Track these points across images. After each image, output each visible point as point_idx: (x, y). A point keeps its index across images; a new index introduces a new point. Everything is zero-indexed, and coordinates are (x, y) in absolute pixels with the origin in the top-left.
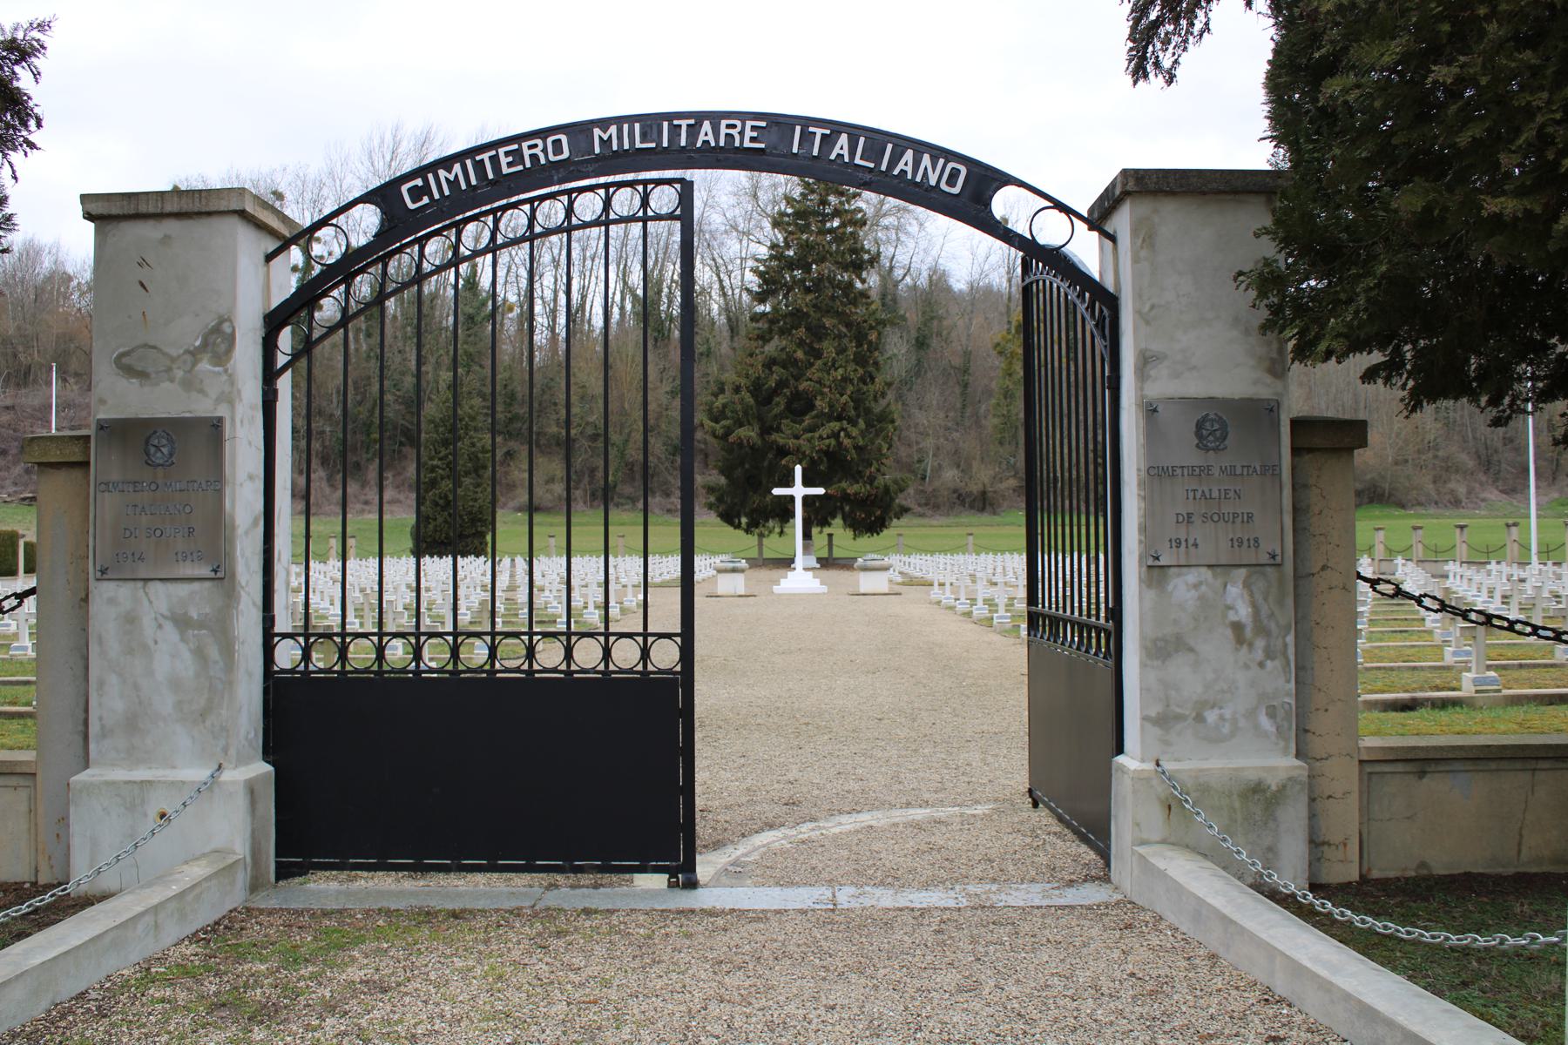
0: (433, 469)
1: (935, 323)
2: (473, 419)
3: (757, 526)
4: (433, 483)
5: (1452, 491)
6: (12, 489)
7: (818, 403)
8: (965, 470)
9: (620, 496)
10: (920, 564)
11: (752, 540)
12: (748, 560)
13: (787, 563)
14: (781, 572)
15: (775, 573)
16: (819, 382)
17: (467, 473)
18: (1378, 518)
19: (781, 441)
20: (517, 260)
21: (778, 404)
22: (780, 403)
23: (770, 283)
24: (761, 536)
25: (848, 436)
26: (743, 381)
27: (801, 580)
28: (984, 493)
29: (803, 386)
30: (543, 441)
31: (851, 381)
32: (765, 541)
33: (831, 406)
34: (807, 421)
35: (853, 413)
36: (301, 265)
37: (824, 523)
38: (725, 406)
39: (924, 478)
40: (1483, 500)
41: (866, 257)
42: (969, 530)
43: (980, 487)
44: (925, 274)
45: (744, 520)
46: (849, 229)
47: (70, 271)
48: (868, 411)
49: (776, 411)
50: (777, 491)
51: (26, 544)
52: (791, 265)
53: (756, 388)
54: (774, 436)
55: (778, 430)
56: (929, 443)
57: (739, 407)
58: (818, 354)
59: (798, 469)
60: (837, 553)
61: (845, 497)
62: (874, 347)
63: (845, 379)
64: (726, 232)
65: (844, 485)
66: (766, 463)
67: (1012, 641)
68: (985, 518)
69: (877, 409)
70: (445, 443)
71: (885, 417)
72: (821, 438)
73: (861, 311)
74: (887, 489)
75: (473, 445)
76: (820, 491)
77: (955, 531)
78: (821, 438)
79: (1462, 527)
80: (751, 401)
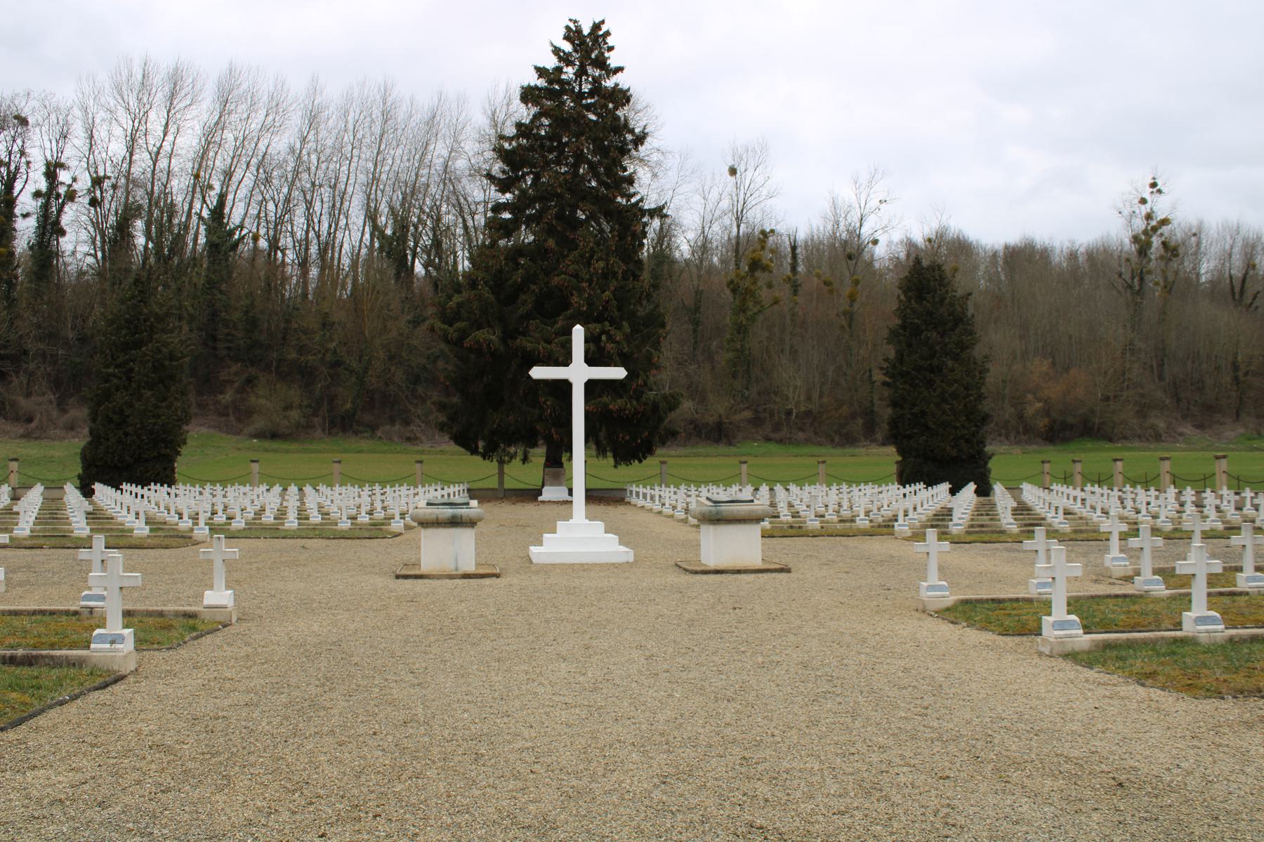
5: (1153, 427)
7: (575, 299)
11: (491, 467)
16: (576, 276)
19: (529, 346)
20: (267, 197)
21: (525, 302)
22: (527, 302)
25: (610, 338)
26: (480, 275)
31: (615, 274)
32: (506, 468)
33: (590, 304)
38: (459, 305)
40: (1181, 434)
41: (629, 137)
45: (481, 444)
49: (522, 310)
53: (498, 282)
54: (521, 342)
55: (524, 334)
68: (722, 449)
74: (655, 407)
75: (159, 351)
80: (492, 297)
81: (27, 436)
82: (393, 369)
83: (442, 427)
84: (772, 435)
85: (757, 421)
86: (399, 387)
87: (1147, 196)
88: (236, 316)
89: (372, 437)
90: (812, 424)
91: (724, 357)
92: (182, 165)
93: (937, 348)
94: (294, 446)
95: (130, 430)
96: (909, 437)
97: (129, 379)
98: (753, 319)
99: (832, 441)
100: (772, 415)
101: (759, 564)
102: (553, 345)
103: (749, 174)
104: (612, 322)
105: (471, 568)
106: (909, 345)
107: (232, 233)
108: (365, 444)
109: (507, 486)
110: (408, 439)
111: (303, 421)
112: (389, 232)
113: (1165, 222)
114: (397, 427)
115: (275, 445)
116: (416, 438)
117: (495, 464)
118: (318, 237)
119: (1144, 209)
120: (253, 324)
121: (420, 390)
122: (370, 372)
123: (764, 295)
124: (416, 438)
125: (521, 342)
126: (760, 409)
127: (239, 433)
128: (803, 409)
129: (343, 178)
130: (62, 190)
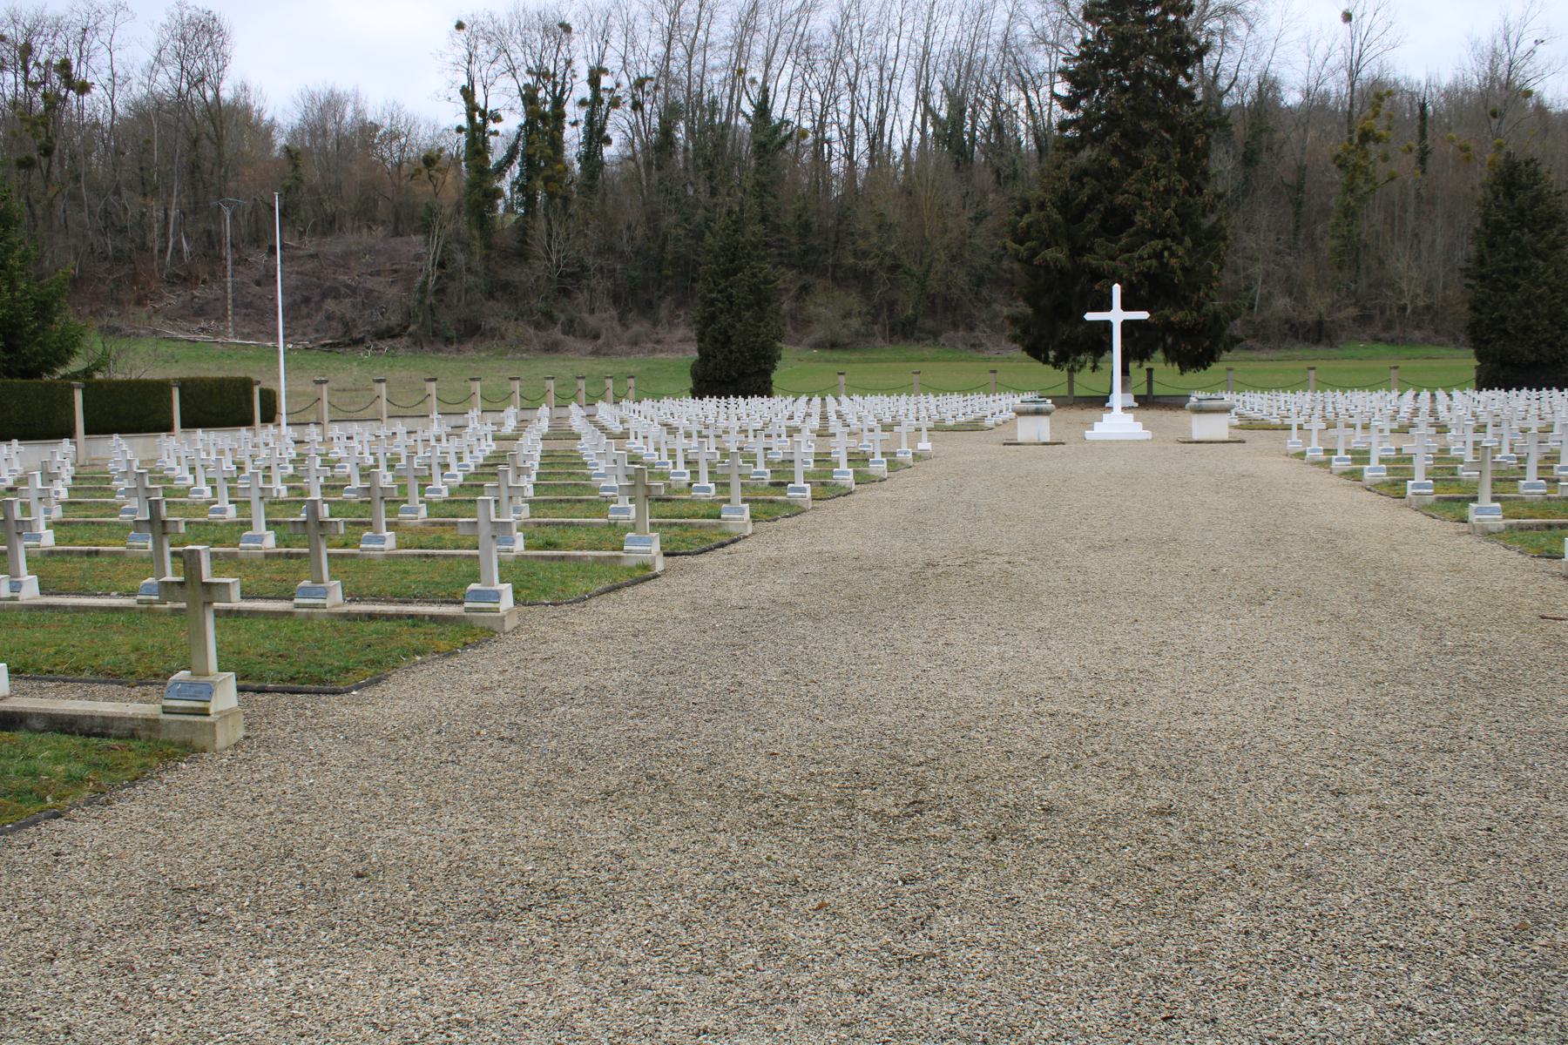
0: (712, 302)
1: (1265, 136)
2: (755, 247)
3: (1066, 361)
4: (712, 318)
6: (312, 336)
7: (1138, 218)
9: (921, 330)
10: (1257, 403)
11: (1062, 375)
12: (1054, 399)
13: (1100, 402)
14: (1095, 412)
16: (1139, 195)
17: (748, 307)
20: (811, 84)
22: (1093, 220)
23: (1082, 78)
24: (1072, 371)
25: (1172, 254)
26: (1048, 197)
27: (1119, 423)
28: (1319, 324)
29: (1120, 199)
30: (840, 274)
32: (1076, 376)
35: (1178, 229)
36: (589, 98)
37: (1143, 356)
38: (1029, 225)
39: (1251, 307)
43: (1315, 317)
44: (1254, 84)
45: (1052, 354)
46: (1172, 17)
47: (370, 118)
48: (1196, 227)
49: (1089, 228)
50: (1090, 316)
51: (262, 392)
52: (1105, 62)
53: (1064, 203)
54: (1088, 259)
55: (1091, 250)
56: (1258, 269)
57: (1044, 226)
58: (1137, 164)
59: (1117, 289)
60: (1158, 390)
61: (1168, 327)
62: (1204, 153)
63: (1169, 191)
64: (1033, 44)
65: (1167, 312)
66: (1078, 289)
67: (1451, 527)
68: (1321, 351)
69: (1207, 222)
70: (727, 274)
71: (1216, 234)
72: (1141, 258)
74: (1216, 318)
75: (754, 275)
76: (1143, 315)
81: (596, 353)
83: (1014, 339)
84: (1382, 335)
85: (1364, 319)
88: (789, 219)
89: (936, 344)
90: (1432, 320)
91: (1329, 245)
92: (718, 59)
94: (856, 356)
95: (734, 347)
96: (1487, 342)
97: (731, 303)
98: (1362, 199)
99: (1456, 340)
100: (1382, 313)
101: (1226, 438)
102: (1118, 263)
103: (1367, 20)
104: (1174, 238)
106: (1492, 245)
107: (777, 129)
108: (927, 352)
110: (973, 346)
111: (863, 329)
112: (943, 114)
114: (961, 333)
115: (836, 355)
116: (981, 345)
117: (1065, 372)
118: (867, 125)
120: (806, 228)
121: (984, 292)
122: (931, 275)
123: (1380, 171)
124: (981, 345)
125: (1090, 260)
126: (1368, 304)
127: (797, 344)
128: (1421, 303)
129: (892, 52)
130: (605, 96)
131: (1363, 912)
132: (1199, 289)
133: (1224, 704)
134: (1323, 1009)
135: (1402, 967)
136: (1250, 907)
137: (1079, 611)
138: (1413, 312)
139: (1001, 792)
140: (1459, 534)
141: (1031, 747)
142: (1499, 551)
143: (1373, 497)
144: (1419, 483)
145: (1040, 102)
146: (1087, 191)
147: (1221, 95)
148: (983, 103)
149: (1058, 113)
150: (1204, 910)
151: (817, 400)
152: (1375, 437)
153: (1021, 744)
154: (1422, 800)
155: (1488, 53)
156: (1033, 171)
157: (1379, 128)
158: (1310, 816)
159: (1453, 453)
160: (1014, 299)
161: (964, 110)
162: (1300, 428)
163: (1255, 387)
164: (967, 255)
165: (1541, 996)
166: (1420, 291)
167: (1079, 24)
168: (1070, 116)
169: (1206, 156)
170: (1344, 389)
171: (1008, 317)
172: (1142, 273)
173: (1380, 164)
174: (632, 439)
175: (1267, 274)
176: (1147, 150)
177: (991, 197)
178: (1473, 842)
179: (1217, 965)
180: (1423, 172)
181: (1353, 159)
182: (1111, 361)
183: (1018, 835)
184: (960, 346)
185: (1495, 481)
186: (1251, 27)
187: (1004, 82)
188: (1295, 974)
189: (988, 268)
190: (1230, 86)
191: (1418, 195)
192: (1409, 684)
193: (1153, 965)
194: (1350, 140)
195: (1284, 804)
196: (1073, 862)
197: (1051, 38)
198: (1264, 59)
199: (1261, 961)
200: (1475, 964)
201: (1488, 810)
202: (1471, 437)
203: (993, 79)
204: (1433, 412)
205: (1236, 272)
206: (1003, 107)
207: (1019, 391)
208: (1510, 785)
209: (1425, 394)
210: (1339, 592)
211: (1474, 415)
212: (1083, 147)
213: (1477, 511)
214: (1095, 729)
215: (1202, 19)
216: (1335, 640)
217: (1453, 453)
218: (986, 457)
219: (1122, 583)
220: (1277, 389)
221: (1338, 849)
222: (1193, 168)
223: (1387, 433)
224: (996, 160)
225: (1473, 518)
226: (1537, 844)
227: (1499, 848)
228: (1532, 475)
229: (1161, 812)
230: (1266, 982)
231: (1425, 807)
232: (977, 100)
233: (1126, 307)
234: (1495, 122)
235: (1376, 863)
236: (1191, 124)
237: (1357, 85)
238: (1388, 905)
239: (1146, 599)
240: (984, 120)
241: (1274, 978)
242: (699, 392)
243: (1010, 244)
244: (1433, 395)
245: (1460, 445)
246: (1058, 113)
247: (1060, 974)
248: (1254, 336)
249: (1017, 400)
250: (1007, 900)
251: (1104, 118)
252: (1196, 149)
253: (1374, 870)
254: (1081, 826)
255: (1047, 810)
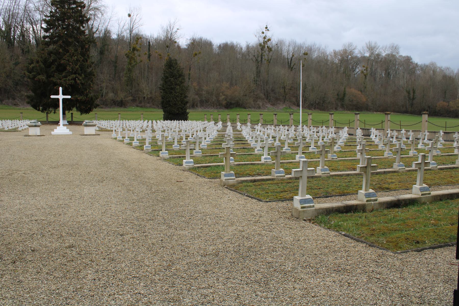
1: (106, 47)
5: (258, 104)
7: (68, 68)
8: (116, 93)
10: (104, 124)
11: (44, 115)
14: (55, 126)
15: (52, 127)
18: (238, 111)
22: (54, 68)
23: (51, 23)
24: (47, 113)
25: (78, 79)
27: (62, 129)
28: (122, 101)
29: (62, 62)
31: (79, 61)
32: (49, 115)
33: (72, 69)
34: (64, 74)
37: (70, 109)
38: (33, 68)
39: (102, 96)
40: (266, 107)
42: (119, 113)
44: (103, 31)
45: (41, 108)
49: (52, 70)
50: (52, 97)
52: (58, 19)
53: (45, 62)
55: (53, 76)
56: (104, 85)
57: (38, 68)
58: (68, 51)
59: (61, 89)
60: (74, 119)
61: (77, 100)
62: (88, 50)
63: (77, 60)
64: (35, 11)
65: (77, 96)
66: (49, 88)
67: (155, 158)
68: (122, 109)
69: (89, 70)
71: (91, 74)
72: (69, 80)
73: (83, 37)
74: (92, 98)
76: (69, 97)
77: (113, 113)
78: (69, 80)
79: (276, 114)
80: (43, 66)
82: (8, 80)
83: (28, 103)
84: (139, 105)
85: (134, 100)
86: (11, 87)
87: (264, 31)
90: (152, 101)
91: (124, 79)
93: (173, 83)
96: (166, 107)
98: (133, 67)
99: (158, 107)
100: (139, 99)
101: (94, 134)
104: (79, 74)
105: (39, 135)
109: (49, 120)
110: (15, 105)
113: (269, 40)
114: (10, 100)
117: (45, 113)
119: (264, 35)
121: (18, 88)
123: (138, 59)
124: (18, 104)
125: (54, 80)
131: (128, 268)
132: (86, 90)
133: (90, 212)
134: (116, 298)
135: (138, 282)
136: (95, 272)
137: (46, 187)
138: (147, 98)
139: (18, 247)
140: (157, 160)
141: (29, 231)
142: (167, 164)
143: (135, 150)
144: (147, 146)
145: (37, 29)
146: (52, 58)
147: (94, 33)
148: (17, 27)
149: (43, 33)
150: (81, 275)
151: (150, 122)
152: (135, 133)
153: (25, 231)
154: (145, 234)
155: (166, 30)
156: (35, 50)
157: (138, 47)
158: (114, 242)
159: (157, 138)
160: (29, 90)
161: (11, 29)
162: (115, 131)
163: (103, 119)
164: (12, 75)
165: (173, 283)
166: (149, 93)
167: (50, 7)
168: (48, 34)
169: (89, 51)
170: (128, 120)
171: (26, 96)
172: (69, 84)
173: (138, 58)
174: (256, 131)
175: (107, 86)
176: (70, 48)
177: (21, 57)
178: (157, 244)
179: (85, 291)
180: (149, 60)
181: (131, 55)
182: (59, 111)
183: (22, 260)
184: (10, 104)
185: (166, 146)
186: (102, 14)
187: (25, 21)
188: (108, 289)
189: (20, 80)
190: (96, 31)
191: (148, 67)
192: (142, 202)
193: (65, 294)
194: (130, 50)
195: (107, 240)
196: (41, 266)
197: (41, 9)
198: (106, 24)
199: (98, 287)
200: (157, 277)
201: (162, 235)
202: (161, 133)
203: (21, 20)
204: (152, 126)
205: (98, 85)
206: (25, 29)
207: (30, 119)
208: (168, 228)
209: (150, 122)
210: (125, 177)
211: (163, 127)
212: (50, 45)
213: (162, 153)
214: (50, 224)
215: (88, 10)
216: (123, 191)
217: (157, 138)
218: (18, 140)
219: (60, 178)
220: (110, 120)
221: (121, 251)
222: (85, 54)
223: (139, 132)
224: (22, 46)
225: (161, 155)
226: (174, 243)
227: (164, 245)
228: (176, 144)
229: (70, 247)
230: (100, 293)
231: (145, 236)
232: (15, 25)
233: (64, 94)
234: (167, 49)
235: (132, 254)
236: (84, 41)
237: (132, 35)
238: (135, 265)
239: (68, 182)
240: (18, 33)
241: (102, 291)
242: (166, 118)
243: (27, 73)
244: (152, 122)
245: (158, 136)
246: (43, 33)
247: (35, 303)
248: (103, 104)
249: (29, 122)
250: (18, 282)
251: (57, 36)
252: (86, 48)
253: (131, 255)
254: (44, 254)
255: (33, 251)
